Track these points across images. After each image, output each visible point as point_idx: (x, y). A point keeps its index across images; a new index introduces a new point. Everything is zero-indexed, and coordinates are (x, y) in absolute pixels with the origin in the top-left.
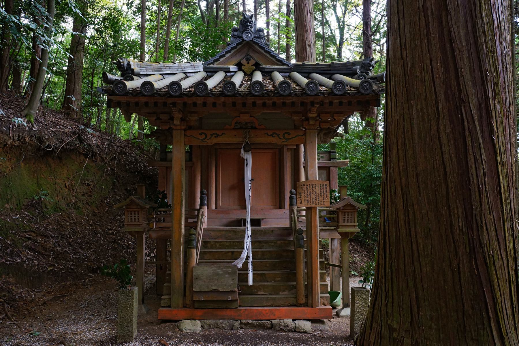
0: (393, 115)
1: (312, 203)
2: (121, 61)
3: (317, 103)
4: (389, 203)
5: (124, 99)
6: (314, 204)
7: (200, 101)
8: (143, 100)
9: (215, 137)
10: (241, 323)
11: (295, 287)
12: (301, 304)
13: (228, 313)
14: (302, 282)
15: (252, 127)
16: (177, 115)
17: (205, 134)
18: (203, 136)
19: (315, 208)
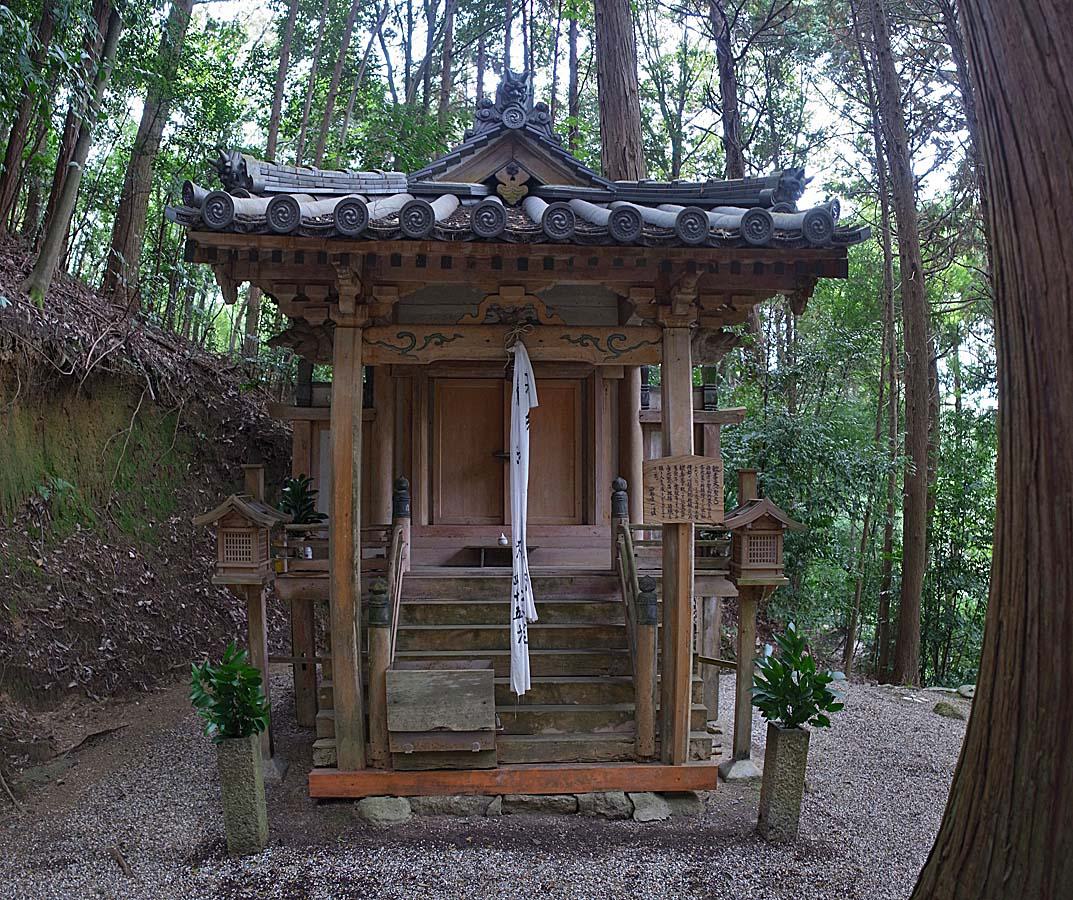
0: (1048, 262)
1: (679, 514)
2: (227, 157)
3: (702, 266)
4: (1047, 561)
5: (223, 242)
6: (687, 517)
7: (409, 251)
8: (269, 244)
9: (437, 344)
10: (504, 802)
11: (632, 716)
12: (645, 757)
13: (474, 779)
14: (650, 705)
15: (529, 320)
16: (349, 288)
17: (411, 335)
18: (406, 342)
19: (687, 526)
